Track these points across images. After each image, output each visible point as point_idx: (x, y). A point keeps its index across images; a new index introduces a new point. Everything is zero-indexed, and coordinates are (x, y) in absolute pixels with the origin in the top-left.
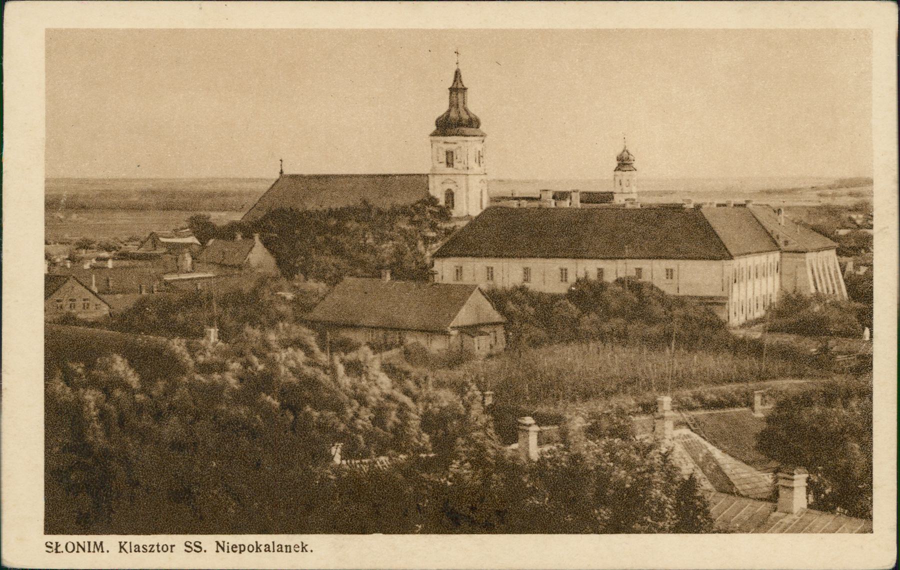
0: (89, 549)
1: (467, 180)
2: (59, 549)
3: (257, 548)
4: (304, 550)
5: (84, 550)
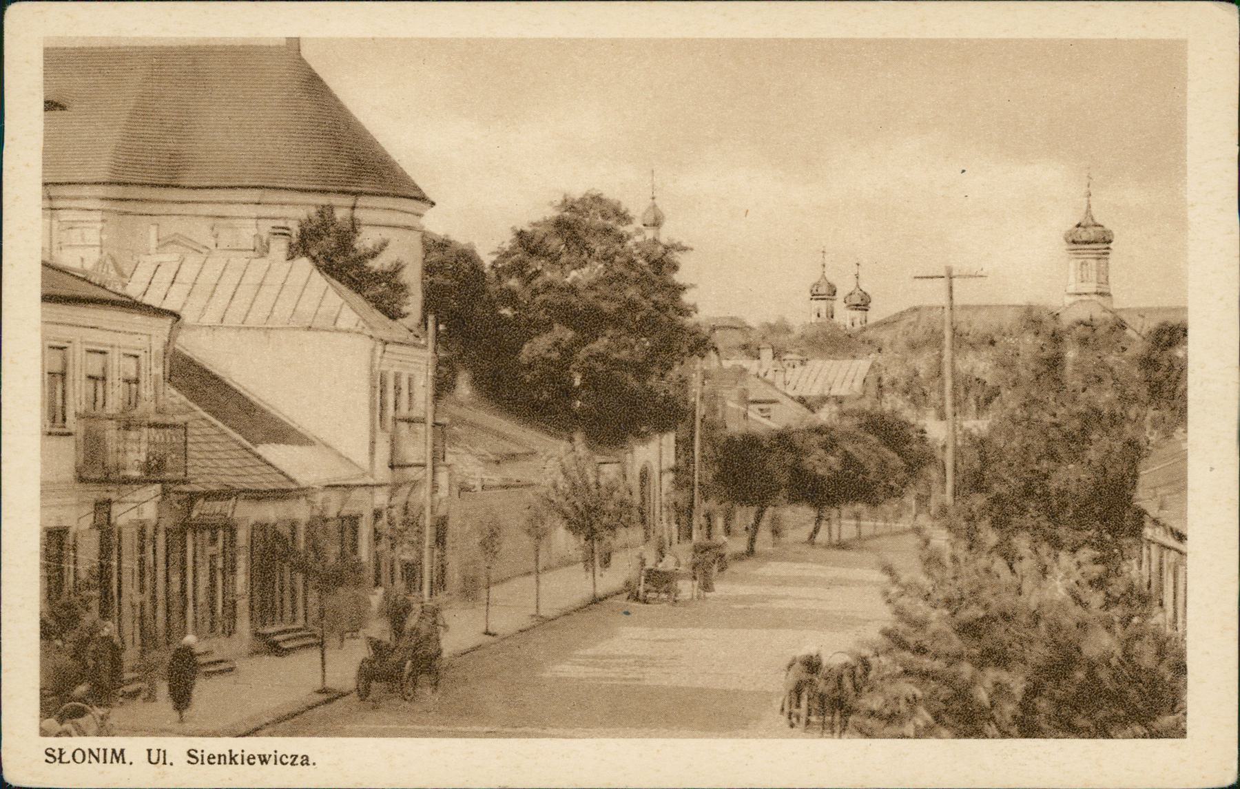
0: (165, 761)
1: (1141, 331)
2: (64, 759)
3: (232, 759)
4: (233, 762)
5: (97, 759)
